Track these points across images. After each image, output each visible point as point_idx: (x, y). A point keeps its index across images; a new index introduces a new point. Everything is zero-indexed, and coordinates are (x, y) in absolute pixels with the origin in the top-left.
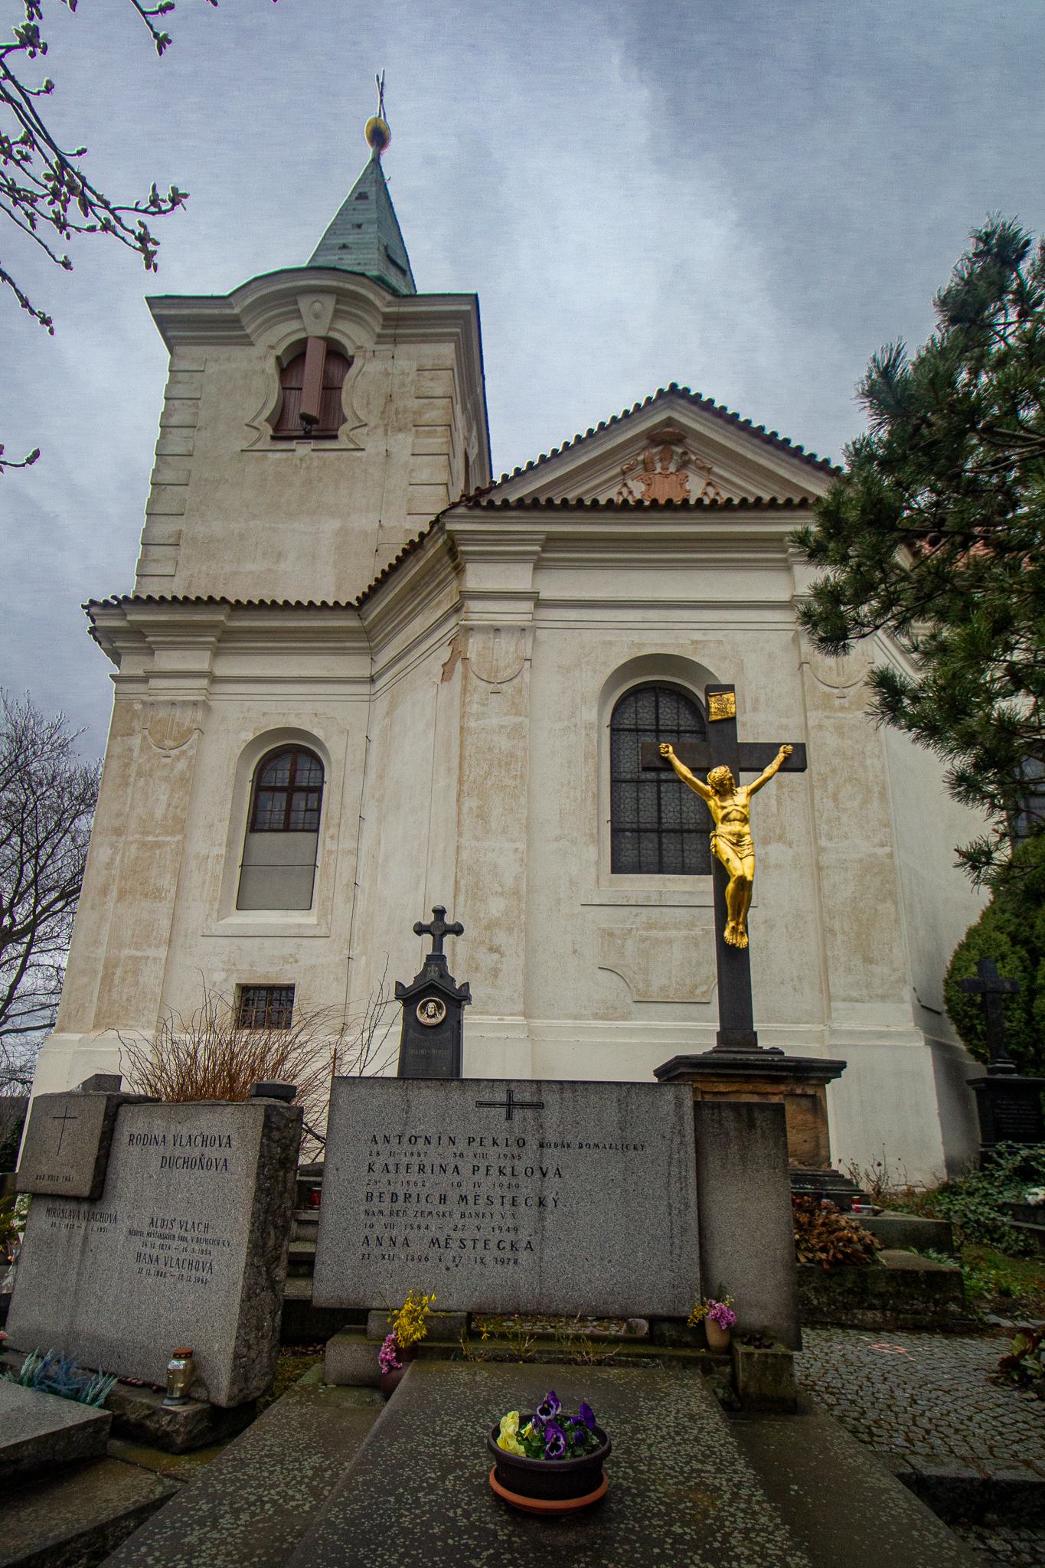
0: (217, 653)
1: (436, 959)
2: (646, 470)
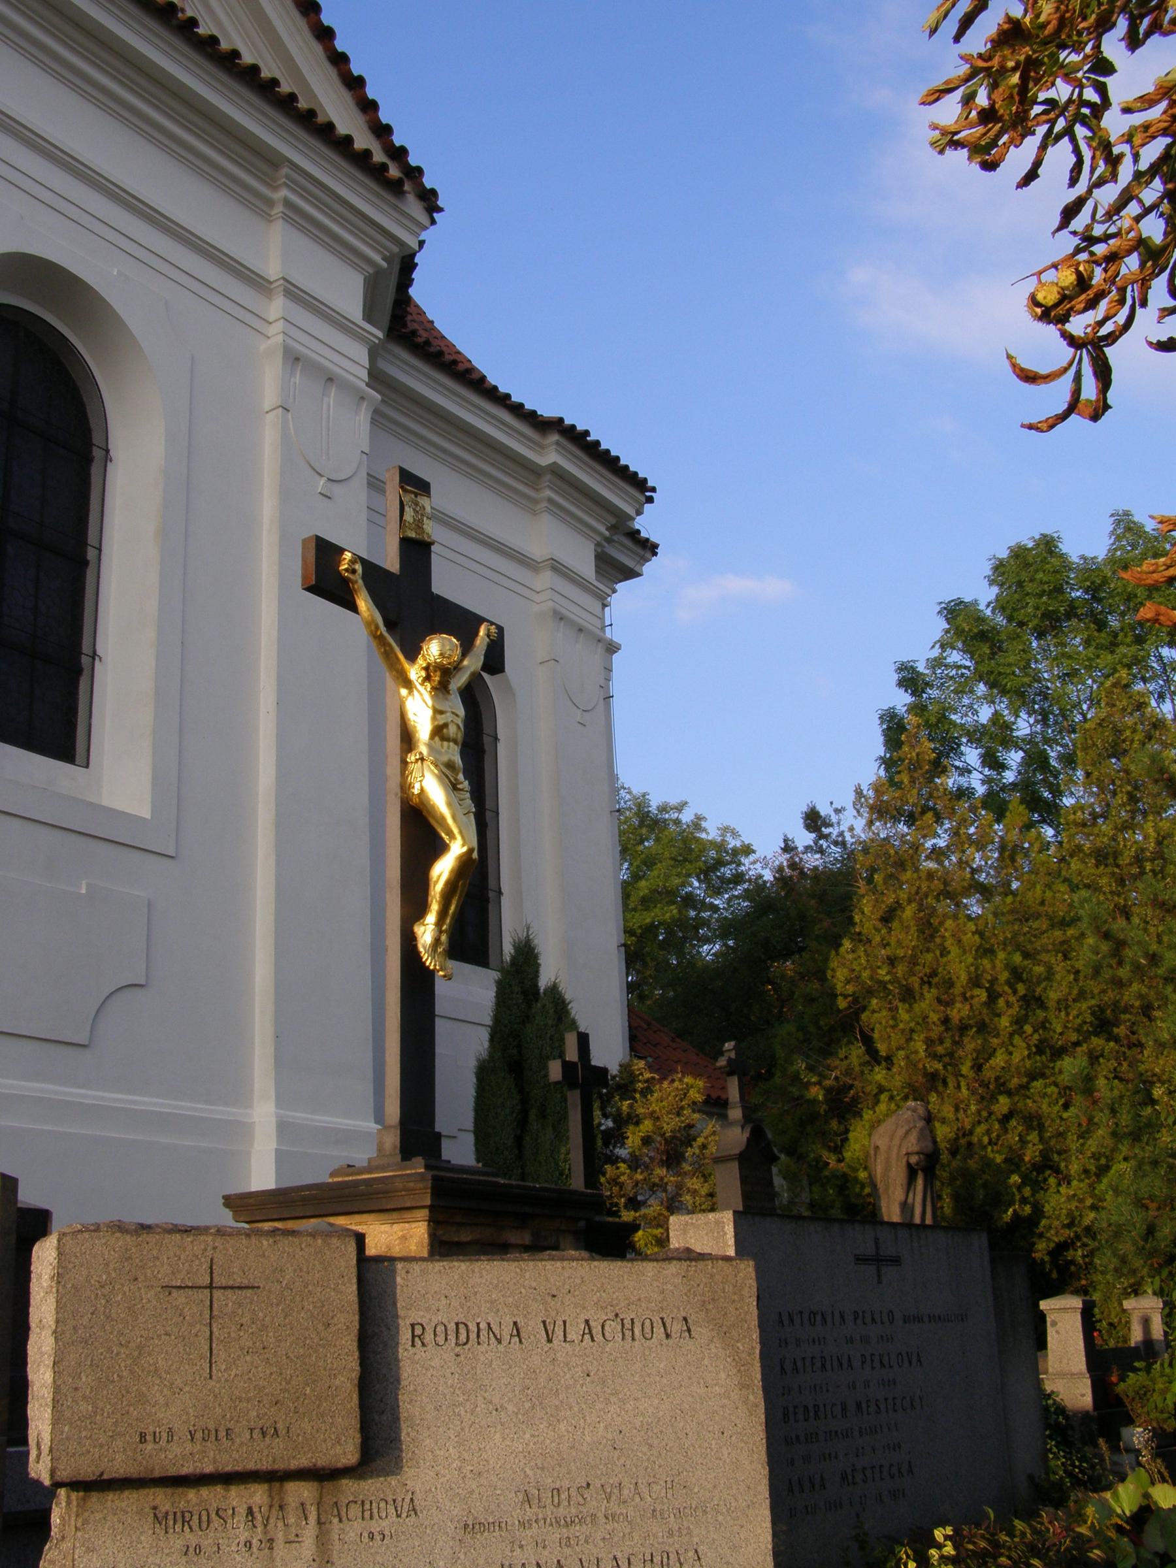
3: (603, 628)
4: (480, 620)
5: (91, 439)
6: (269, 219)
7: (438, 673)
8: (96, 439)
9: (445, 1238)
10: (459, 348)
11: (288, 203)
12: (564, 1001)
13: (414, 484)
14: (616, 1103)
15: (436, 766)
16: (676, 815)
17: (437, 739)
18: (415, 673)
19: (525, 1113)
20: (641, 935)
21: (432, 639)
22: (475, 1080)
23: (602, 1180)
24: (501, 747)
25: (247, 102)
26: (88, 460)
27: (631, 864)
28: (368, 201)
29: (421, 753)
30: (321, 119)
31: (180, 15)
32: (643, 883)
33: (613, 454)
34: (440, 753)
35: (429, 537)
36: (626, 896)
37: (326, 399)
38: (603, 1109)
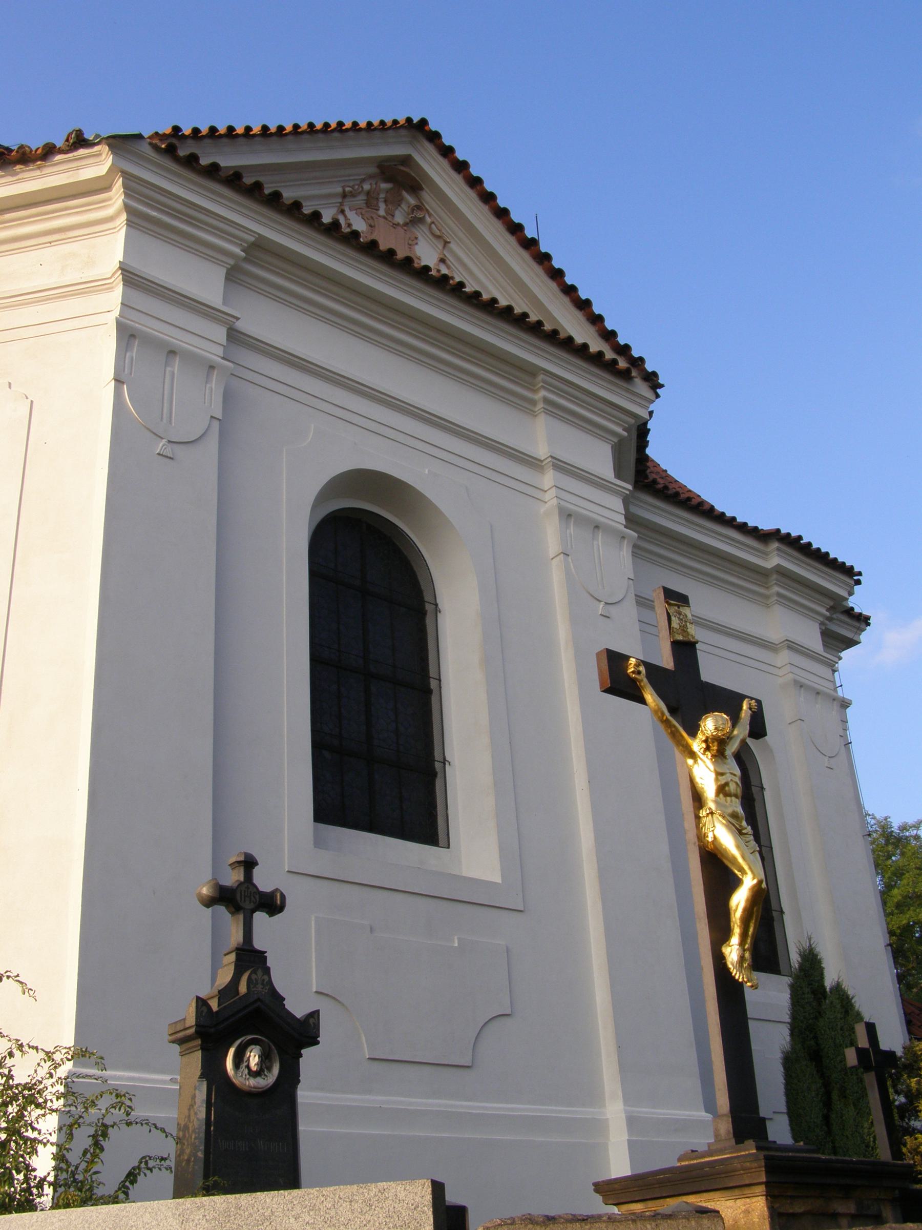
0: (234, 276)
1: (250, 958)
2: (368, 204)
3: (835, 689)
4: (742, 697)
5: (423, 598)
6: (534, 414)
7: (716, 744)
8: (427, 597)
9: (782, 1210)
10: (689, 487)
11: (546, 400)
12: (848, 997)
13: (675, 598)
14: (905, 1081)
15: (724, 817)
16: (915, 832)
17: (721, 796)
18: (697, 745)
19: (828, 1094)
20: (901, 935)
21: (707, 718)
22: (782, 1069)
23: (904, 1150)
24: (767, 794)
25: (506, 332)
26: (422, 613)
27: (883, 877)
28: (608, 389)
29: (710, 809)
30: (562, 335)
31: (451, 282)
32: (895, 891)
33: (823, 551)
34: (725, 806)
35: (694, 638)
36: (884, 903)
37: (595, 543)
38: (894, 1086)
